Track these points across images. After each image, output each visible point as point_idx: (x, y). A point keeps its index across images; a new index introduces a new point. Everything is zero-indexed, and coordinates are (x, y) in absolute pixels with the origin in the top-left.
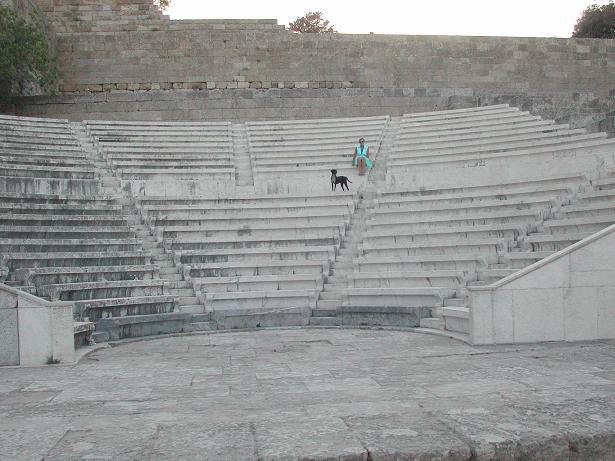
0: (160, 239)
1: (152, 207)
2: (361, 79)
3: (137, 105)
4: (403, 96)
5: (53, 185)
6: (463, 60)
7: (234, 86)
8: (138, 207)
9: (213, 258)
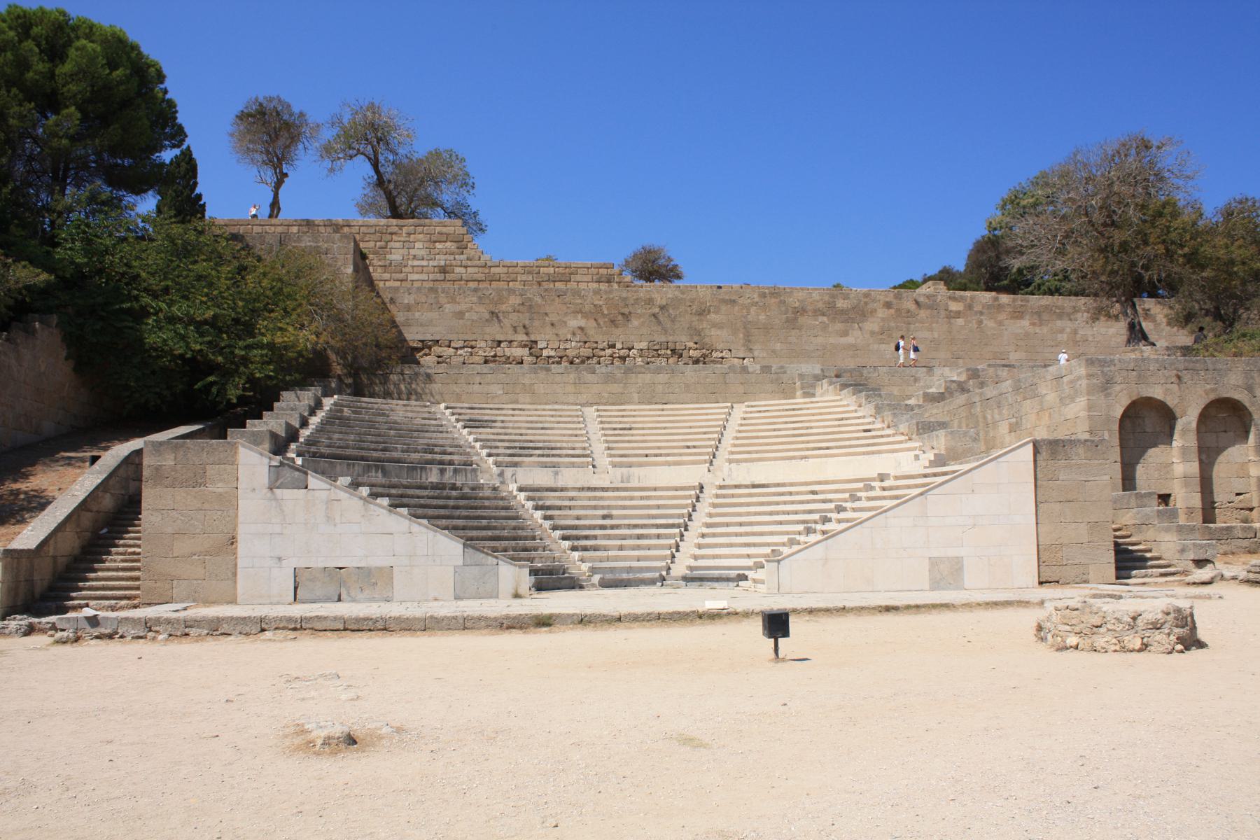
2: (707, 340)
3: (478, 379)
5: (442, 471)
6: (821, 319)
9: (586, 538)
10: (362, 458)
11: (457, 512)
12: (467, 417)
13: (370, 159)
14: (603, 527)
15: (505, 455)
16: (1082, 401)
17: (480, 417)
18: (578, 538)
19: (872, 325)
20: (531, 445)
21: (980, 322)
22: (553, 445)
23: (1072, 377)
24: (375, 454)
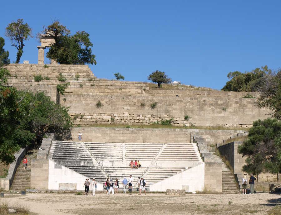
0: (108, 175)
1: (106, 169)
2: (171, 114)
3: (94, 131)
4: (176, 131)
6: (212, 107)
7: (124, 115)
8: (103, 168)
11: (88, 173)
12: (91, 146)
22: (113, 155)
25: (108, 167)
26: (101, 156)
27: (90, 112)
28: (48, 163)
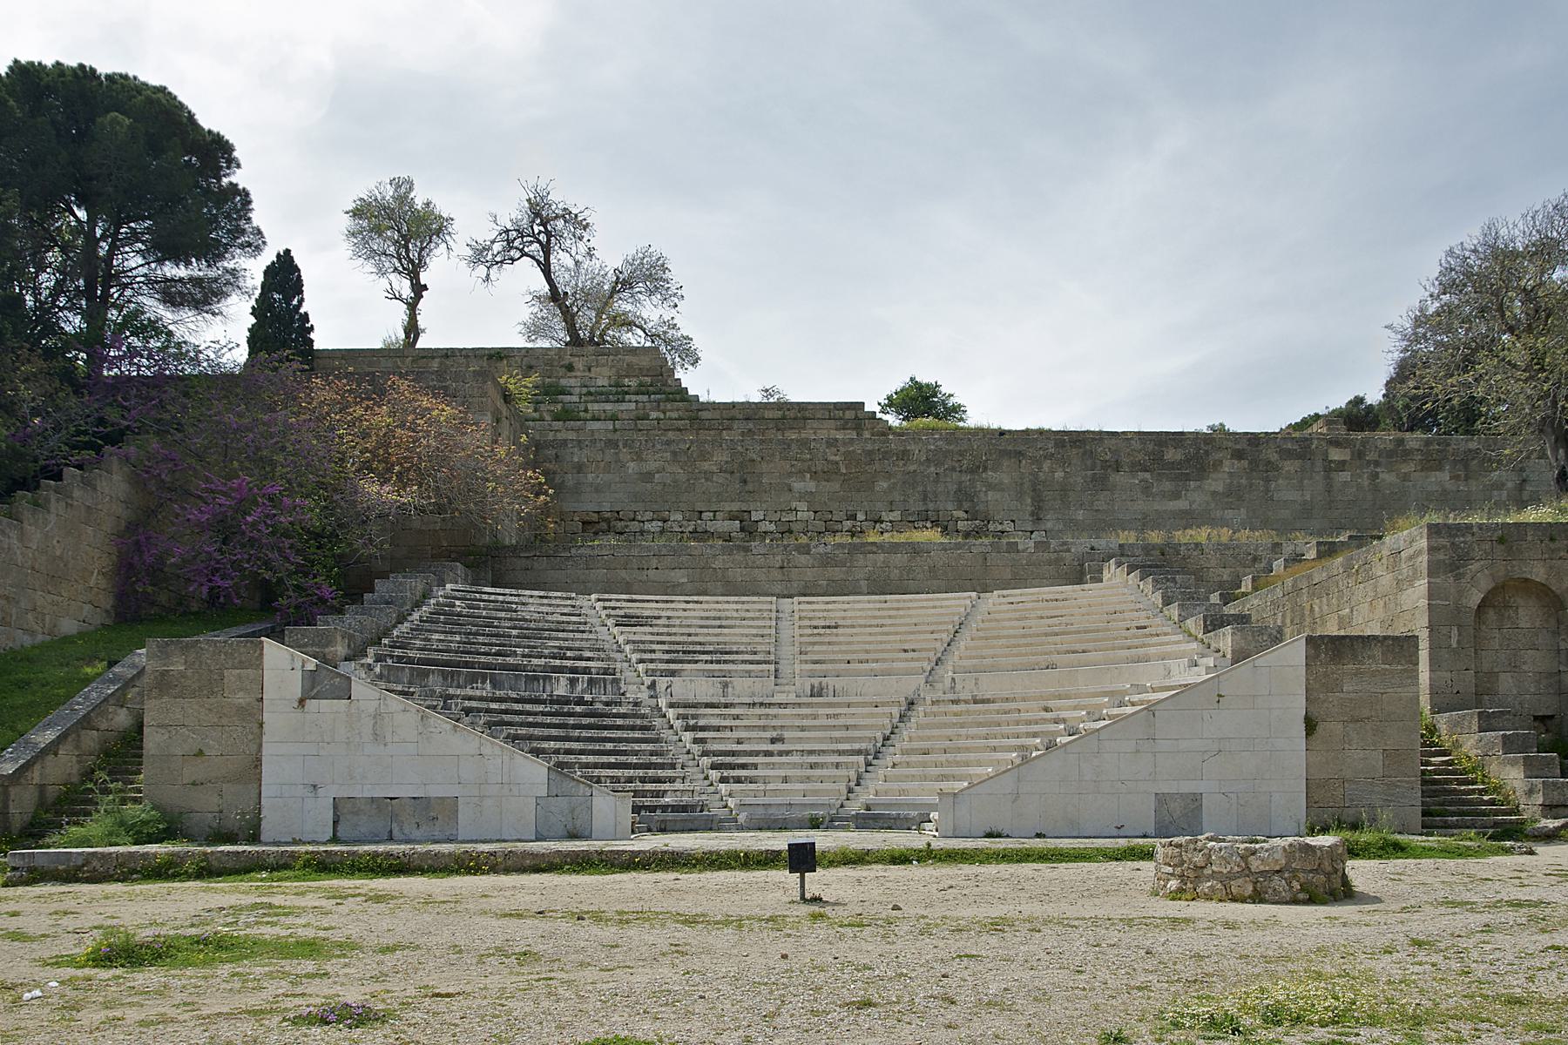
2: (981, 507)
3: (654, 562)
5: (573, 682)
9: (743, 766)
10: (467, 665)
12: (621, 613)
13: (539, 262)
14: (768, 754)
15: (662, 661)
16: (1422, 584)
17: (638, 612)
18: (732, 767)
19: (1216, 483)
20: (698, 648)
21: (1375, 476)
23: (1411, 551)
24: (483, 659)
25: (694, 706)
26: (668, 652)
27: (655, 507)
28: (258, 663)
